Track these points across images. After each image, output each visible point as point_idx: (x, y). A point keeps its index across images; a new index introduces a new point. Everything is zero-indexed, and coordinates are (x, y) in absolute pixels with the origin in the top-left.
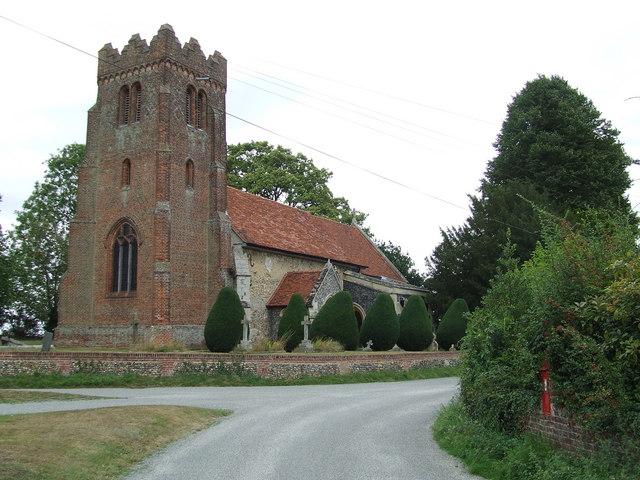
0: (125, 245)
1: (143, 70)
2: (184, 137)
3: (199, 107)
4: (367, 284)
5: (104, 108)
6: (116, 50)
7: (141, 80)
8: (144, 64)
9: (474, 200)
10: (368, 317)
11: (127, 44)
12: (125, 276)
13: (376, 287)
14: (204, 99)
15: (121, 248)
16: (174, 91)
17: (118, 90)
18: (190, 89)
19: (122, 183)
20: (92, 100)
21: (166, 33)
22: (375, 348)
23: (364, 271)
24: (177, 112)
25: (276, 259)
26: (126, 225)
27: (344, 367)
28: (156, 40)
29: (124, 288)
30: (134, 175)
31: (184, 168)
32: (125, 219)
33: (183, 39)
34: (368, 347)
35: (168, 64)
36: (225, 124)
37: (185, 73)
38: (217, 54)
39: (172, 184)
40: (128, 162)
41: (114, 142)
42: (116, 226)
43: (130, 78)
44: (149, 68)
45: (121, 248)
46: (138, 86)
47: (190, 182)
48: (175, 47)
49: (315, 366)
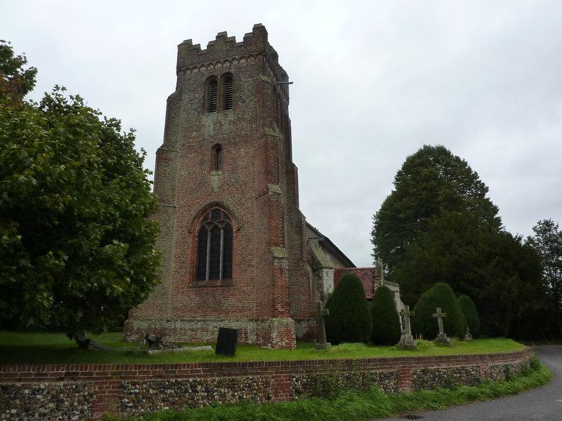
0: (215, 229)
5: (186, 97)
7: (233, 71)
19: (211, 169)
26: (216, 210)
29: (214, 275)
40: (218, 148)
42: (204, 210)
43: (219, 70)
44: (243, 61)
46: (228, 78)
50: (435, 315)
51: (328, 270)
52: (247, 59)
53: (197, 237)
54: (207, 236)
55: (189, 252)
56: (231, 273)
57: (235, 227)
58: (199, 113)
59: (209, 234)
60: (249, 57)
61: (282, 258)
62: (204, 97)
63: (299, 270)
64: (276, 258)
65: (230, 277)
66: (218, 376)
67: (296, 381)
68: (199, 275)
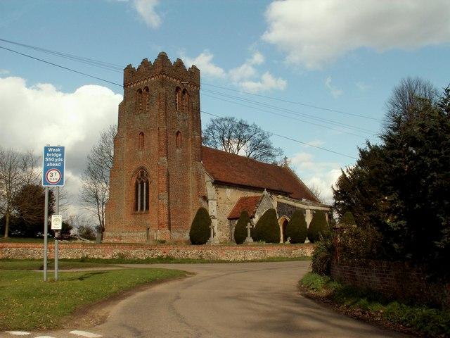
0: (142, 183)
15: (139, 185)
21: (163, 57)
29: (142, 209)
33: (173, 60)
38: (194, 67)
40: (142, 134)
43: (143, 83)
45: (139, 185)
54: (5, 228)
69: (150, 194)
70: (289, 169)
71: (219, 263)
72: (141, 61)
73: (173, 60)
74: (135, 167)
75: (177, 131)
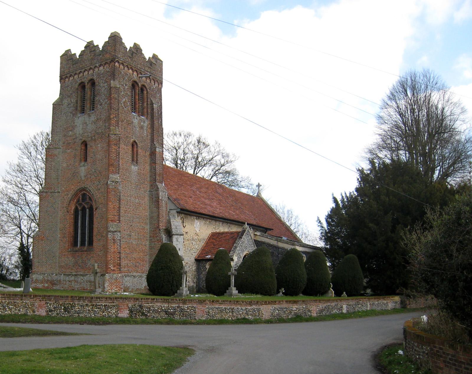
0: (84, 209)
1: (96, 70)
2: (130, 123)
3: (142, 99)
4: (273, 242)
5: (65, 102)
6: (75, 54)
7: (95, 78)
8: (97, 65)
9: (361, 171)
10: (271, 271)
11: (83, 49)
12: (83, 234)
13: (281, 245)
14: (145, 92)
15: (80, 213)
16: (122, 85)
17: (77, 86)
18: (134, 84)
19: (81, 161)
20: (55, 95)
21: (115, 39)
22: (285, 294)
23: (270, 232)
24: (124, 103)
25: (203, 222)
26: (84, 194)
27: (267, 311)
28: (82, 53)
29: (83, 244)
30: (90, 154)
31: (130, 148)
32: (84, 189)
33: (128, 44)
34: (281, 293)
35: (117, 64)
36: (161, 113)
37: (130, 71)
38: (155, 57)
39: (121, 161)
40: (85, 144)
41: (74, 127)
42: (76, 195)
43: (87, 76)
44: (101, 68)
45: (80, 213)
46: (93, 83)
47: (135, 159)
48: (123, 50)
49: (241, 310)
50: (229, 273)
51: (179, 237)
52: (104, 67)
53: (73, 215)
54: (78, 214)
55: (67, 226)
56: (93, 241)
57: (94, 208)
58: (73, 115)
59: (87, 210)
60: (105, 64)
61: (116, 231)
62: (77, 101)
63: (156, 237)
64: (110, 231)
65: (92, 244)
66: (8, 300)
67: (50, 305)
68: (75, 243)
69: (95, 226)
70: (262, 200)
71: (198, 324)
72: (85, 44)
73: (128, 44)
74: (74, 188)
75: (132, 140)
